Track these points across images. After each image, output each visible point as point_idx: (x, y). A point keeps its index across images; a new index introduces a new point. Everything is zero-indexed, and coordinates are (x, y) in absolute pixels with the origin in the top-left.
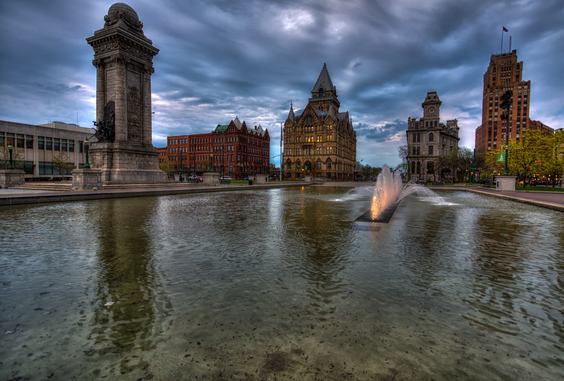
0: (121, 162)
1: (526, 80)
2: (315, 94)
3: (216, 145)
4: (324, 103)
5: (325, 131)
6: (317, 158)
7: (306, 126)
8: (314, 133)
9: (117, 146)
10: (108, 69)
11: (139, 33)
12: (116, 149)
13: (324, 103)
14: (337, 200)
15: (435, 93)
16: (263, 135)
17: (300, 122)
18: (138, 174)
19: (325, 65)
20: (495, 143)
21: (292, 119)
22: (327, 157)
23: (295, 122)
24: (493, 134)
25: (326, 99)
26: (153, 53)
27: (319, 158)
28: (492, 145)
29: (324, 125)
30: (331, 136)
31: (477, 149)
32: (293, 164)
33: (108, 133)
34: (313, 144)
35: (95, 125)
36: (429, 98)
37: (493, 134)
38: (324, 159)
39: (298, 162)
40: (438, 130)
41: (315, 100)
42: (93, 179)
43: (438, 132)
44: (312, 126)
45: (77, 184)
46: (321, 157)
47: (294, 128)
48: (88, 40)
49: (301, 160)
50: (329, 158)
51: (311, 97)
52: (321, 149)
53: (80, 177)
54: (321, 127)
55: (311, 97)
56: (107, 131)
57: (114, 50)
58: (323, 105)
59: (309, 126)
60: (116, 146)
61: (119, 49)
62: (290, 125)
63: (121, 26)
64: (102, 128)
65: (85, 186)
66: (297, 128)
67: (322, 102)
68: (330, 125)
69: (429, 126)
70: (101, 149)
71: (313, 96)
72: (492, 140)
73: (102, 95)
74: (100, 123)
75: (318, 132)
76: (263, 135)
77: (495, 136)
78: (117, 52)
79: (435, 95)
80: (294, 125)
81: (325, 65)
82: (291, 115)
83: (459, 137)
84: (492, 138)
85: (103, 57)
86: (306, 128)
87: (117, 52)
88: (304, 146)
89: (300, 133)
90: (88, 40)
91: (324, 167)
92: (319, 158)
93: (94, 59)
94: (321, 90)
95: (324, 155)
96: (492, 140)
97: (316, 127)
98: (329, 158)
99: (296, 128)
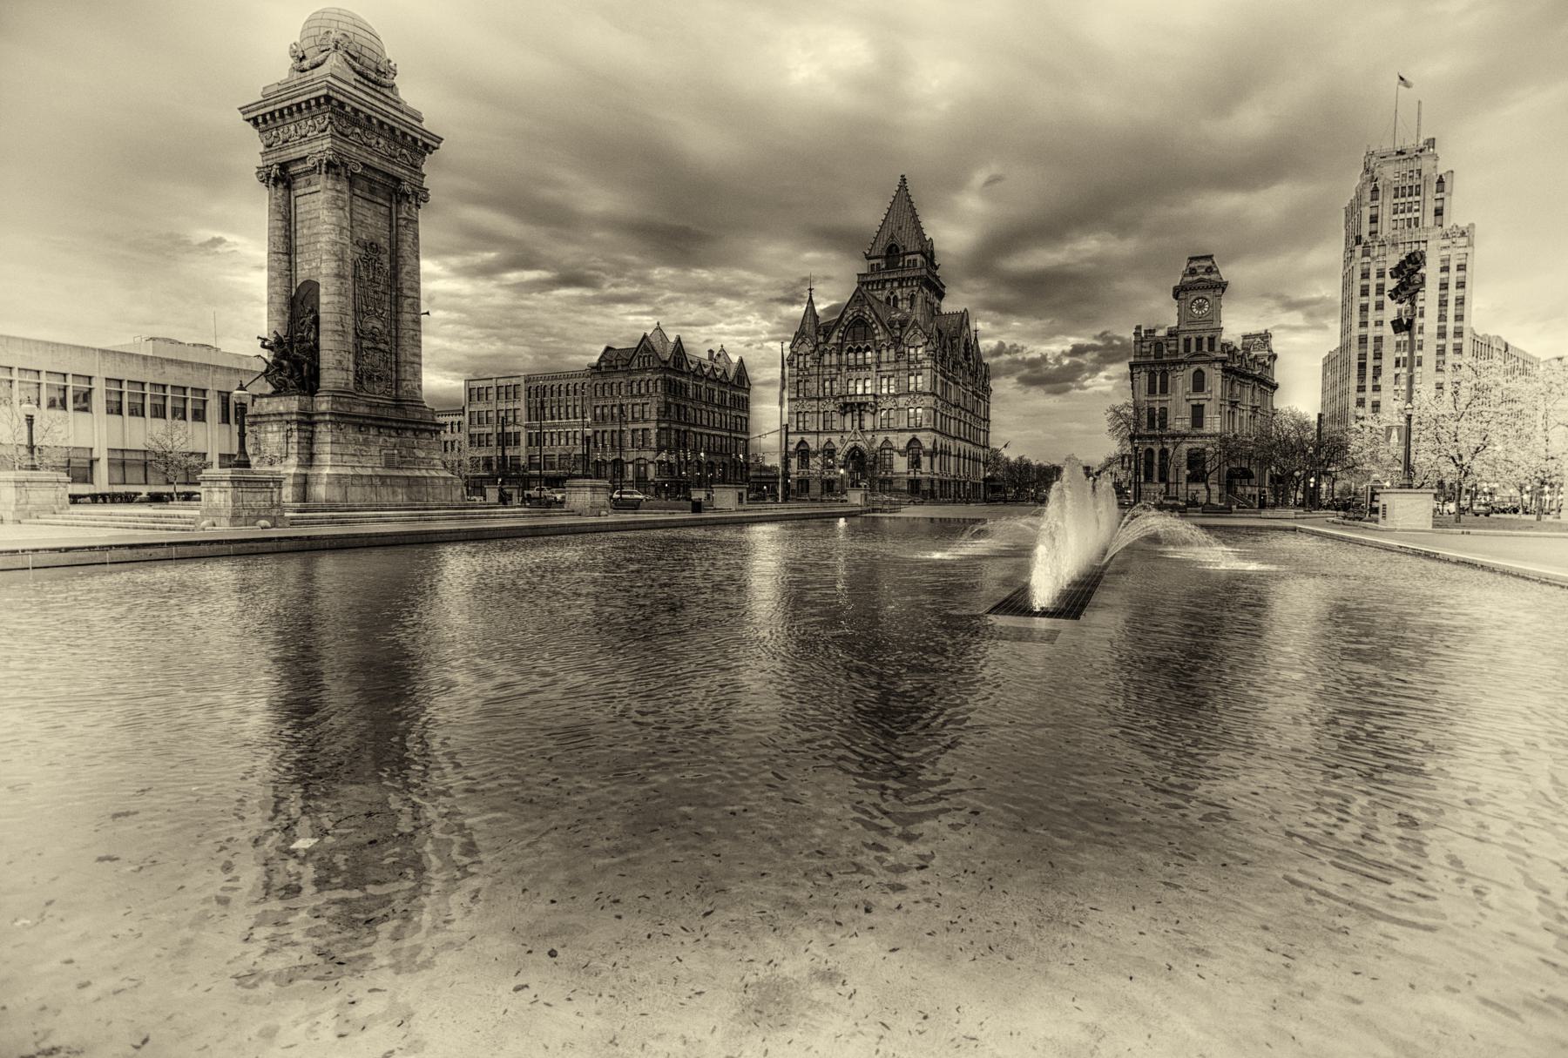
0: (337, 449)
1: (1463, 224)
2: (875, 262)
3: (601, 403)
4: (900, 286)
5: (903, 365)
8: (874, 368)
10: (299, 192)
11: (386, 91)
12: (323, 414)
13: (900, 286)
14: (937, 556)
16: (731, 375)
17: (834, 340)
18: (383, 484)
22: (908, 436)
23: (821, 339)
26: (426, 146)
32: (815, 454)
33: (301, 371)
34: (871, 399)
35: (263, 346)
37: (1370, 372)
38: (900, 441)
39: (830, 452)
40: (1216, 360)
41: (876, 278)
42: (259, 497)
43: (1218, 365)
45: (214, 511)
48: (244, 110)
49: (838, 445)
53: (223, 490)
54: (892, 352)
56: (297, 364)
60: (323, 404)
61: (332, 136)
63: (337, 72)
64: (284, 355)
65: (235, 518)
66: (827, 356)
69: (1193, 350)
70: (281, 414)
73: (284, 265)
74: (279, 341)
75: (884, 368)
76: (731, 375)
77: (1375, 378)
78: (327, 143)
80: (817, 346)
81: (904, 180)
82: (810, 320)
85: (285, 159)
86: (851, 355)
87: (327, 143)
88: (846, 404)
89: (834, 371)
90: (244, 110)
91: (901, 464)
92: (886, 440)
97: (879, 351)
98: (914, 439)
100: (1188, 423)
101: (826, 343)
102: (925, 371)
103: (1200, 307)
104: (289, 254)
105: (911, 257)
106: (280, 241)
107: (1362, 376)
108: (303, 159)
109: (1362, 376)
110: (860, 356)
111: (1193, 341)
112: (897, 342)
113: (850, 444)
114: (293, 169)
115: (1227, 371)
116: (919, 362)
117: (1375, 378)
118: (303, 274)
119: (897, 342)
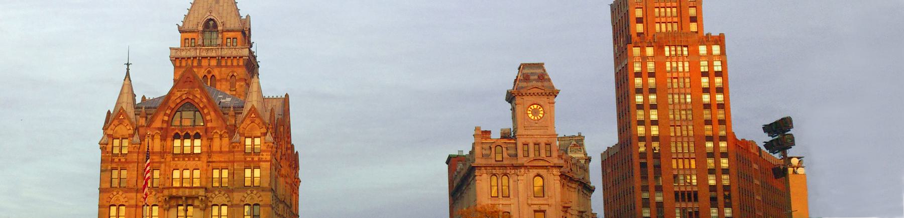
1: (715, 33)
4: (219, 65)
5: (239, 156)
7: (177, 136)
8: (204, 158)
13: (219, 65)
17: (157, 123)
20: (659, 198)
21: (131, 112)
23: (142, 121)
24: (651, 171)
25: (226, 52)
28: (653, 205)
29: (237, 137)
30: (257, 172)
34: (202, 192)
36: (526, 78)
37: (651, 171)
40: (555, 166)
41: (192, 53)
43: (556, 172)
44: (197, 136)
47: (136, 139)
51: (178, 44)
54: (226, 140)
55: (178, 44)
58: (216, 72)
59: (187, 136)
67: (214, 62)
69: (532, 155)
71: (184, 41)
72: (652, 189)
75: (215, 158)
77: (656, 178)
79: (539, 71)
80: (137, 129)
82: (126, 98)
83: (592, 185)
86: (177, 143)
88: (172, 197)
94: (210, 26)
96: (652, 189)
99: (142, 138)
101: (148, 126)
102: (263, 165)
103: (535, 112)
105: (231, 34)
107: (644, 177)
109: (644, 177)
111: (531, 146)
112: (232, 131)
115: (563, 176)
119: (232, 131)
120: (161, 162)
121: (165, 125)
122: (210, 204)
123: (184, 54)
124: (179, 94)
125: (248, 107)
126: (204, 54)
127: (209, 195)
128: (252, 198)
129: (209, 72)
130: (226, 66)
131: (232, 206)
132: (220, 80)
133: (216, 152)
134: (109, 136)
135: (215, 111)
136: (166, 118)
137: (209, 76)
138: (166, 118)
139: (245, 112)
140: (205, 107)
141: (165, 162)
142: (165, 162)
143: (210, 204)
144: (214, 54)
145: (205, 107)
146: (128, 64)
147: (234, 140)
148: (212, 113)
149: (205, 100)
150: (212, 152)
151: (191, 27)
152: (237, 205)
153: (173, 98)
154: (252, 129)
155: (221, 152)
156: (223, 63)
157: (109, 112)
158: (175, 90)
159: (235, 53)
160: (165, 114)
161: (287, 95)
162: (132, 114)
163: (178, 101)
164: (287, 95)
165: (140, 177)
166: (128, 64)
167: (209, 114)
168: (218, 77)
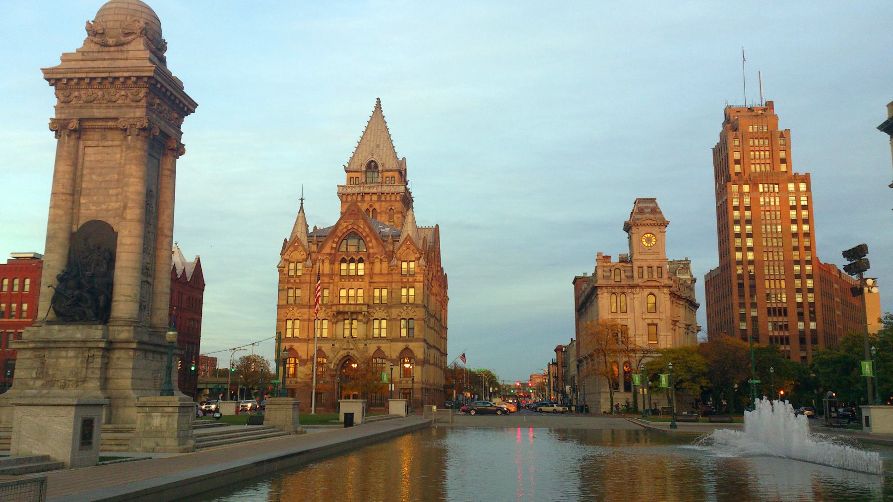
1: (802, 173)
4: (379, 200)
5: (396, 278)
6: (372, 348)
8: (367, 279)
9: (123, 333)
10: (90, 143)
15: (653, 200)
16: (189, 275)
17: (327, 250)
19: (379, 101)
20: (754, 313)
21: (304, 240)
22: (401, 346)
23: (314, 248)
24: (747, 290)
25: (385, 189)
27: (379, 348)
30: (412, 292)
31: (714, 327)
34: (365, 308)
37: (747, 290)
40: (665, 286)
41: (356, 190)
43: (666, 291)
46: (385, 346)
47: (309, 263)
48: (46, 71)
50: (407, 348)
52: (384, 323)
57: (128, 106)
58: (376, 206)
62: (299, 255)
67: (375, 198)
68: (408, 262)
69: (646, 277)
71: (350, 179)
72: (748, 305)
73: (70, 204)
76: (189, 275)
77: (752, 296)
78: (140, 113)
80: (309, 255)
84: (747, 300)
86: (344, 266)
88: (339, 313)
90: (46, 71)
92: (379, 348)
93: (54, 117)
94: (372, 166)
95: (393, 340)
96: (748, 305)
98: (407, 348)
100: (645, 338)
101: (319, 252)
102: (417, 285)
103: (649, 240)
104: (73, 195)
105: (389, 174)
106: (66, 179)
107: (742, 295)
108: (116, 119)
109: (742, 295)
110: (352, 266)
112: (390, 256)
113: (343, 353)
114: (87, 124)
115: (672, 294)
116: (413, 276)
117: (752, 296)
118: (89, 210)
119: (390, 256)
120: (330, 283)
121: (333, 251)
122: (372, 318)
123: (349, 191)
124: (345, 225)
125: (404, 236)
126: (367, 191)
127: (371, 310)
128: (408, 313)
129: (371, 206)
130: (386, 201)
131: (391, 320)
132: (380, 213)
133: (377, 274)
134: (286, 260)
135: (376, 239)
136: (334, 245)
137: (371, 210)
138: (334, 245)
139: (402, 239)
140: (368, 235)
141: (333, 283)
142: (333, 283)
143: (372, 318)
144: (375, 191)
145: (368, 235)
146: (302, 199)
147: (392, 264)
148: (374, 241)
149: (367, 230)
150: (373, 274)
151: (355, 168)
152: (395, 319)
153: (340, 228)
154: (407, 254)
155: (381, 274)
156: (383, 198)
157: (286, 240)
158: (342, 222)
159: (393, 190)
160: (334, 242)
161: (437, 226)
162: (305, 242)
163: (345, 230)
164: (437, 226)
165: (312, 295)
166: (302, 199)
167: (371, 241)
168: (378, 211)
